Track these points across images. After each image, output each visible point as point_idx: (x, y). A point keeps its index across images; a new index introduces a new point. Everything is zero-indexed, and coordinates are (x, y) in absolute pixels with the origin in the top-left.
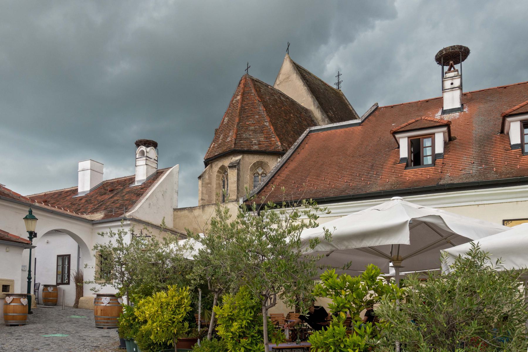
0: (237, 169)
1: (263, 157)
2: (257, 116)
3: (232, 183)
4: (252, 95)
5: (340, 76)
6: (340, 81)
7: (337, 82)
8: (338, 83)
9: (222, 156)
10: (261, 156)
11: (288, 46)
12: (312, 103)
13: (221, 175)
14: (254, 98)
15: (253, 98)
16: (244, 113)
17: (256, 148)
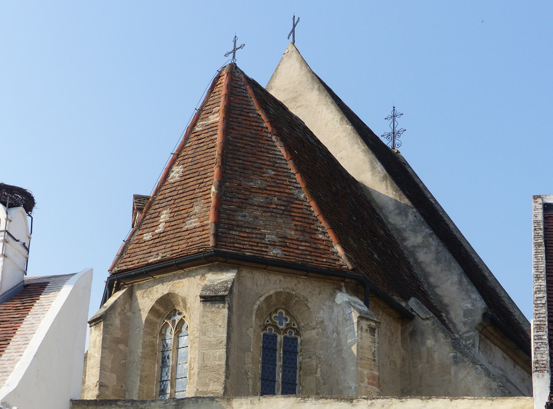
0: (227, 305)
1: (294, 281)
2: (270, 171)
3: (539, 341)
4: (251, 115)
5: (397, 119)
6: (397, 129)
7: (390, 131)
8: (394, 135)
9: (173, 265)
10: (289, 279)
11: (294, 26)
12: (367, 166)
13: (159, 321)
14: (257, 124)
15: (254, 124)
16: (232, 158)
17: (275, 252)
